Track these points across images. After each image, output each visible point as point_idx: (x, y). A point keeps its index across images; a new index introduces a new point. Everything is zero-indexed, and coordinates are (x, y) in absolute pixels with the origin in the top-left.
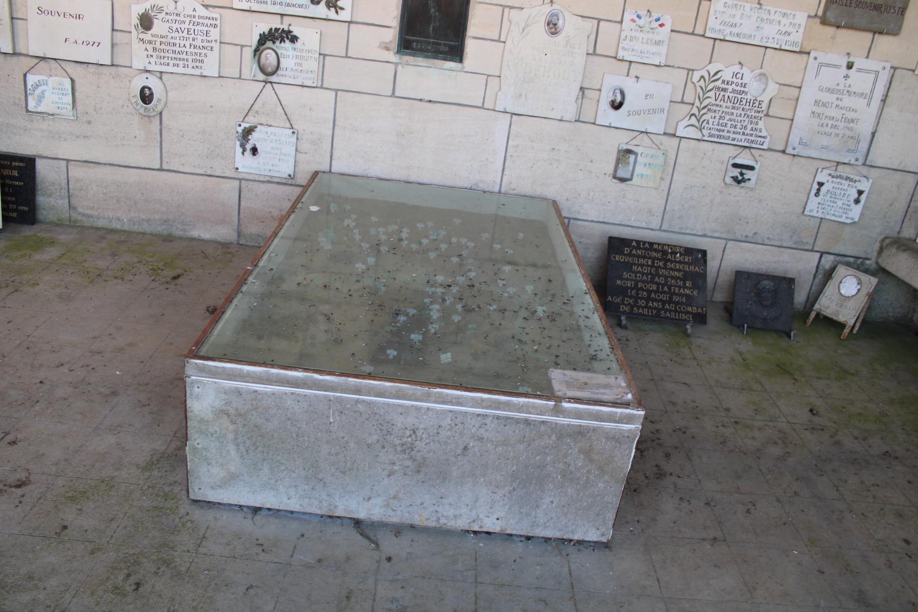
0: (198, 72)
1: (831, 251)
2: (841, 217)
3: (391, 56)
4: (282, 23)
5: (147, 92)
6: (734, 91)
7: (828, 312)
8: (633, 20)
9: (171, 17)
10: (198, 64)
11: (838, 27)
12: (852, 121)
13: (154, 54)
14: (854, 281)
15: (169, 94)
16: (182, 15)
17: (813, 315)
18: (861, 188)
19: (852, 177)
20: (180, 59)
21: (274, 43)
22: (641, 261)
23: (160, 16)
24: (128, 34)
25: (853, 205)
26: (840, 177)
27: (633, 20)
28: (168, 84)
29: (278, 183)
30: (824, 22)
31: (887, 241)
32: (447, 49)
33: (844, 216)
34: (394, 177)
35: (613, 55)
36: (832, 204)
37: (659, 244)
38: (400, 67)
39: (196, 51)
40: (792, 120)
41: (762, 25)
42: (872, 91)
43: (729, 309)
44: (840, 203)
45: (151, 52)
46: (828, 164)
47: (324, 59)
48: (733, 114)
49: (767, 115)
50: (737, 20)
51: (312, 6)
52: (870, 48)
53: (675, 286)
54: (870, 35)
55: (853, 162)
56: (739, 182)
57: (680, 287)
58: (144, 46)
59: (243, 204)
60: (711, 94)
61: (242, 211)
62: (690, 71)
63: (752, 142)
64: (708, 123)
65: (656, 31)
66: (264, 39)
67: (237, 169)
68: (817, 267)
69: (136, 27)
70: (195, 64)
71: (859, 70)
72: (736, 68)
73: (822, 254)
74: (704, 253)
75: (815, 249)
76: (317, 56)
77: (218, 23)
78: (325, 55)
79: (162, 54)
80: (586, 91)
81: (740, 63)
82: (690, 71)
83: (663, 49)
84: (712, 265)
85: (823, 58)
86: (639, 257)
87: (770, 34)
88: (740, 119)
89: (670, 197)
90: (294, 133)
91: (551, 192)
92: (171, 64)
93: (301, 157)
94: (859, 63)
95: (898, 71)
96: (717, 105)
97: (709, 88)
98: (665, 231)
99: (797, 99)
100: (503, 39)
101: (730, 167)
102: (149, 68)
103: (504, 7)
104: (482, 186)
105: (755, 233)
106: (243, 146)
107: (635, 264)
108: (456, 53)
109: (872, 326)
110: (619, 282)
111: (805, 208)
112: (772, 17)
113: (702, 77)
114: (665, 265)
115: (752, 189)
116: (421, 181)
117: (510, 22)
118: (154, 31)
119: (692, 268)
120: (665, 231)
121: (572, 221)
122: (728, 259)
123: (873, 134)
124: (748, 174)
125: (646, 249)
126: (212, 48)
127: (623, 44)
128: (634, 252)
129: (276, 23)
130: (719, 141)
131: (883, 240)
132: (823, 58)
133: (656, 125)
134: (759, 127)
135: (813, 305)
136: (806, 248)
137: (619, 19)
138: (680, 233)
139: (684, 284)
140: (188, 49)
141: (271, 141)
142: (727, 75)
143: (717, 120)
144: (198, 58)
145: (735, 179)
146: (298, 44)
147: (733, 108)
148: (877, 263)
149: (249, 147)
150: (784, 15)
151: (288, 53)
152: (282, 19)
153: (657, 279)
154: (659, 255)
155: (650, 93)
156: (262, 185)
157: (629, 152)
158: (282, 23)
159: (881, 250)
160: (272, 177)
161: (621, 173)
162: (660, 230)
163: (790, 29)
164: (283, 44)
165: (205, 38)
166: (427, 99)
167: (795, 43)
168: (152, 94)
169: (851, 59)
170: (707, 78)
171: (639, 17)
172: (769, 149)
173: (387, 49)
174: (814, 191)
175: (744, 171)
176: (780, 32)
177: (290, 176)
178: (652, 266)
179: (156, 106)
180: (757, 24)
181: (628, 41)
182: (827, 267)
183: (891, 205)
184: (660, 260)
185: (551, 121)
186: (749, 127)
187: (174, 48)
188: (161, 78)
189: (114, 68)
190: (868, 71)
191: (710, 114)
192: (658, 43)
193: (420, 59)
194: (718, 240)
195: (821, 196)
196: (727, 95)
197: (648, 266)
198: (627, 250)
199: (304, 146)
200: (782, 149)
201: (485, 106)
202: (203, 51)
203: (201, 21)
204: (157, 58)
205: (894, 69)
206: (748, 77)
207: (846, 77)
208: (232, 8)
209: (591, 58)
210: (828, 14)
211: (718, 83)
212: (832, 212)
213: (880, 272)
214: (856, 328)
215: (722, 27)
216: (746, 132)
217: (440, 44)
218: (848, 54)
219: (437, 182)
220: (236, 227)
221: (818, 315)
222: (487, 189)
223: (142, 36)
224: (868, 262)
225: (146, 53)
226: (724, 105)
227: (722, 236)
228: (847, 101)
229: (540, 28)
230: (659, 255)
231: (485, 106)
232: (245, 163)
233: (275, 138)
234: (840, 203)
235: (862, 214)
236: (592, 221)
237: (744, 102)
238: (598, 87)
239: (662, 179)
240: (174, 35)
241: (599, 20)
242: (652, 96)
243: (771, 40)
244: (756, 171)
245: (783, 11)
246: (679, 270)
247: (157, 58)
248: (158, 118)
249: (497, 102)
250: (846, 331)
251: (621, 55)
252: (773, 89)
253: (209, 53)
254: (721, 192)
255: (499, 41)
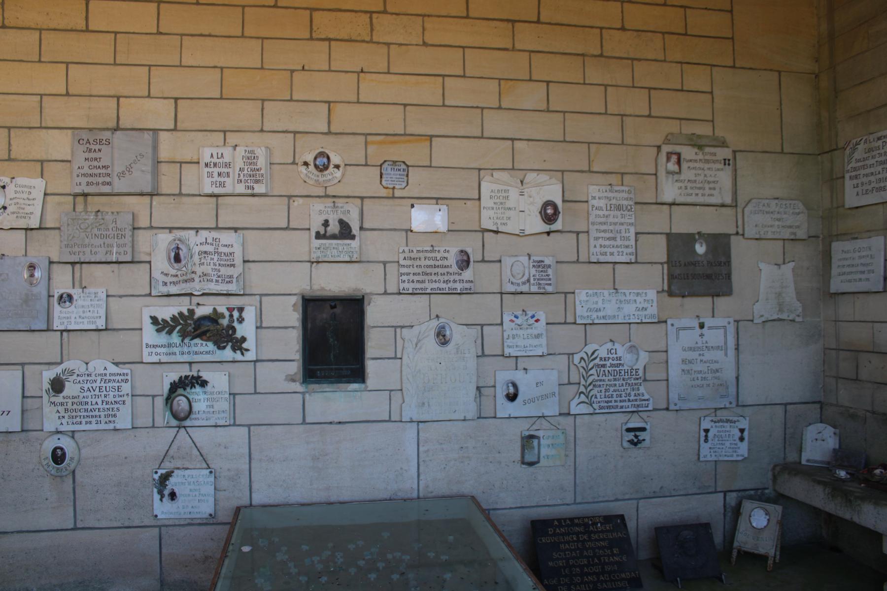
0: (111, 426)
1: (733, 489)
2: (732, 456)
3: (298, 387)
4: (191, 371)
5: (59, 452)
6: (612, 365)
7: (748, 548)
8: (512, 321)
9: (83, 378)
10: (110, 419)
11: (683, 297)
12: (717, 371)
13: (66, 415)
14: (762, 512)
15: (83, 451)
16: (93, 375)
17: (735, 554)
18: (742, 427)
19: (731, 418)
20: (92, 416)
21: (185, 389)
22: (566, 538)
23: (71, 378)
24: (39, 400)
25: (739, 443)
26: (721, 421)
27: (512, 321)
28: (80, 442)
29: (200, 524)
30: (671, 294)
31: (778, 469)
32: (349, 372)
33: (735, 454)
34: (314, 500)
35: (500, 353)
36: (721, 446)
37: (579, 518)
38: (307, 395)
39: (108, 406)
40: (667, 380)
41: (621, 306)
42: (726, 343)
43: (657, 565)
44: (728, 444)
45: (63, 414)
46: (708, 412)
47: (234, 398)
48: (615, 385)
49: (645, 380)
50: (600, 305)
51: (218, 352)
52: (713, 309)
53: (605, 556)
54: (710, 299)
55: (728, 405)
56: (635, 444)
57: (608, 556)
58: (56, 409)
59: (164, 551)
60: (593, 372)
61: (163, 559)
62: (570, 355)
63: (638, 406)
64: (596, 397)
65: (533, 326)
66: (174, 387)
67: (156, 516)
68: (725, 506)
69: (47, 392)
70: (107, 420)
71: (710, 328)
72: (609, 345)
73: (725, 493)
74: (622, 517)
75: (718, 490)
76: (227, 396)
77: (129, 377)
78: (234, 395)
79: (74, 414)
80: (482, 389)
81: (611, 341)
82: (570, 355)
83: (543, 341)
84: (631, 525)
85: (678, 323)
86: (563, 534)
87: (630, 311)
88: (622, 388)
89: (577, 471)
90: (211, 472)
91: (467, 488)
92: (84, 422)
93: (221, 495)
94: (708, 322)
95: (740, 323)
96: (601, 380)
97: (590, 366)
98: (580, 503)
99: (667, 362)
100: (399, 356)
101: (624, 433)
102: (62, 428)
103: (395, 327)
104: (401, 495)
105: (662, 488)
106: (161, 493)
107: (562, 543)
108: (358, 374)
109: (793, 551)
110: (551, 564)
111: (699, 455)
112: (628, 298)
113: (582, 358)
114: (590, 537)
115: (649, 448)
116: (341, 499)
117: (403, 340)
118: (64, 393)
119: (615, 534)
120: (580, 503)
121: (491, 512)
122: (645, 516)
123: (737, 378)
124: (642, 435)
125: (568, 526)
126: (124, 402)
127: (508, 342)
128: (558, 531)
129: (185, 371)
130: (608, 409)
131: (774, 469)
132: (678, 323)
133: (551, 408)
134: (640, 392)
135: (732, 542)
136: (710, 490)
137: (499, 322)
138: (594, 502)
139: (612, 551)
140: (100, 406)
141: (189, 484)
142: (603, 353)
143: (603, 394)
144: (111, 413)
145: (631, 442)
146: (209, 388)
147: (615, 380)
148: (775, 490)
149: (166, 492)
150: (638, 294)
151: (199, 397)
152: (191, 367)
153: (585, 553)
154: (582, 529)
155: (539, 381)
156: (182, 529)
157: (532, 437)
158: (191, 371)
159: (775, 478)
160: (192, 519)
161: (529, 458)
162: (575, 503)
163: (646, 305)
164: (193, 390)
165: (116, 393)
166: (336, 420)
167: (653, 316)
168: (64, 454)
169: (702, 320)
170: (586, 358)
171: (516, 317)
172: (655, 410)
173: (293, 380)
174: (702, 439)
175: (638, 433)
176: (638, 309)
177: (211, 515)
178: (578, 541)
179: (69, 465)
180: (617, 306)
181: (511, 340)
182: (733, 503)
183: (770, 436)
184: (584, 533)
185: (455, 423)
186: (633, 393)
187: (86, 407)
188: (73, 437)
189: (24, 434)
190: (717, 328)
191: (596, 389)
192: (538, 336)
193: (325, 385)
194: (630, 502)
195: (710, 441)
196: (606, 370)
197: (574, 541)
198: (550, 531)
199: (223, 483)
200: (665, 406)
201: (393, 419)
202: (116, 406)
203: (112, 378)
204: (69, 417)
205: (737, 321)
206: (621, 351)
207: (702, 335)
208: (142, 363)
209: (481, 359)
210: (673, 287)
211: (597, 361)
212: (724, 453)
213: (779, 498)
214: (778, 557)
215: (589, 314)
216: (631, 398)
217: (342, 369)
218: (698, 316)
219: (357, 499)
220: (158, 577)
221: (739, 551)
222: (406, 497)
223: (53, 399)
224: (767, 491)
225: (58, 414)
226: (607, 378)
227: (632, 496)
228: (708, 355)
229: (431, 343)
230: (582, 529)
231: (393, 419)
232: (163, 509)
233: (192, 480)
234: (728, 444)
235: (749, 450)
236: (511, 508)
237: (623, 372)
238: (492, 384)
239: (567, 456)
240: (85, 394)
241: (482, 326)
242: (541, 383)
243: (632, 317)
244: (648, 431)
245: (636, 291)
246: (603, 540)
247: (69, 417)
248: (71, 477)
249: (403, 414)
250: (770, 562)
251: (507, 351)
252: (644, 357)
253: (121, 407)
254: (622, 457)
255: (395, 358)
